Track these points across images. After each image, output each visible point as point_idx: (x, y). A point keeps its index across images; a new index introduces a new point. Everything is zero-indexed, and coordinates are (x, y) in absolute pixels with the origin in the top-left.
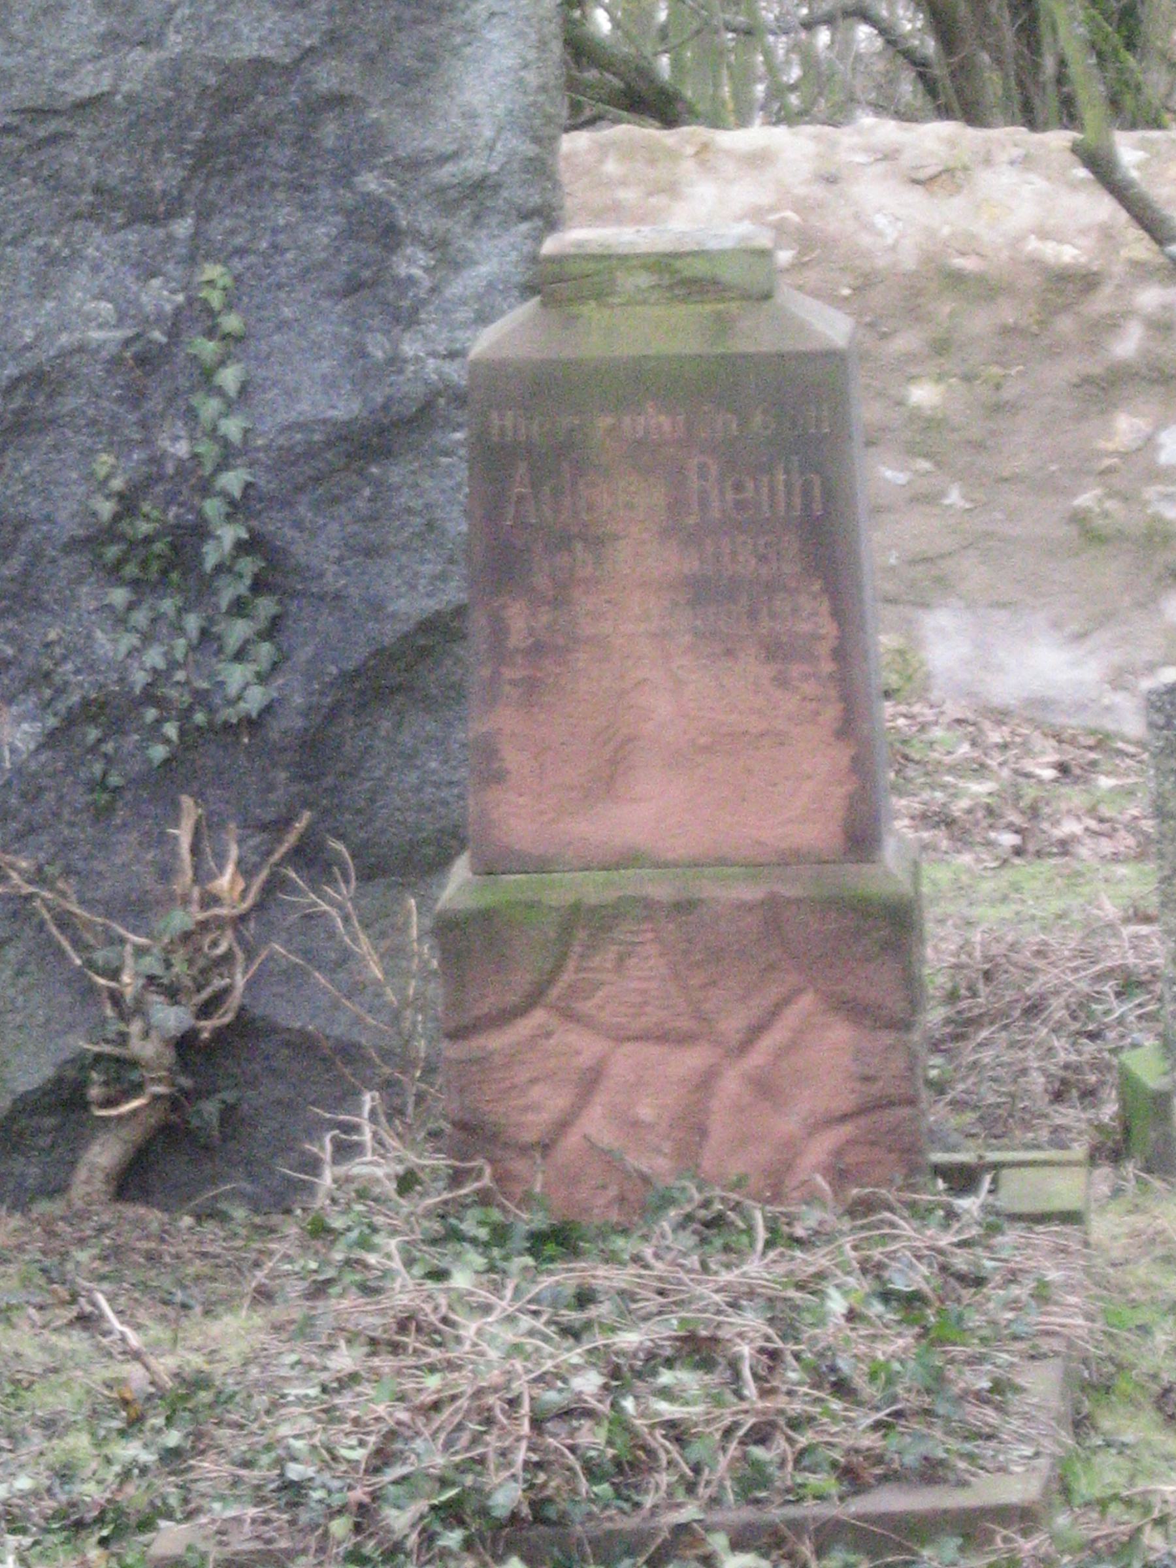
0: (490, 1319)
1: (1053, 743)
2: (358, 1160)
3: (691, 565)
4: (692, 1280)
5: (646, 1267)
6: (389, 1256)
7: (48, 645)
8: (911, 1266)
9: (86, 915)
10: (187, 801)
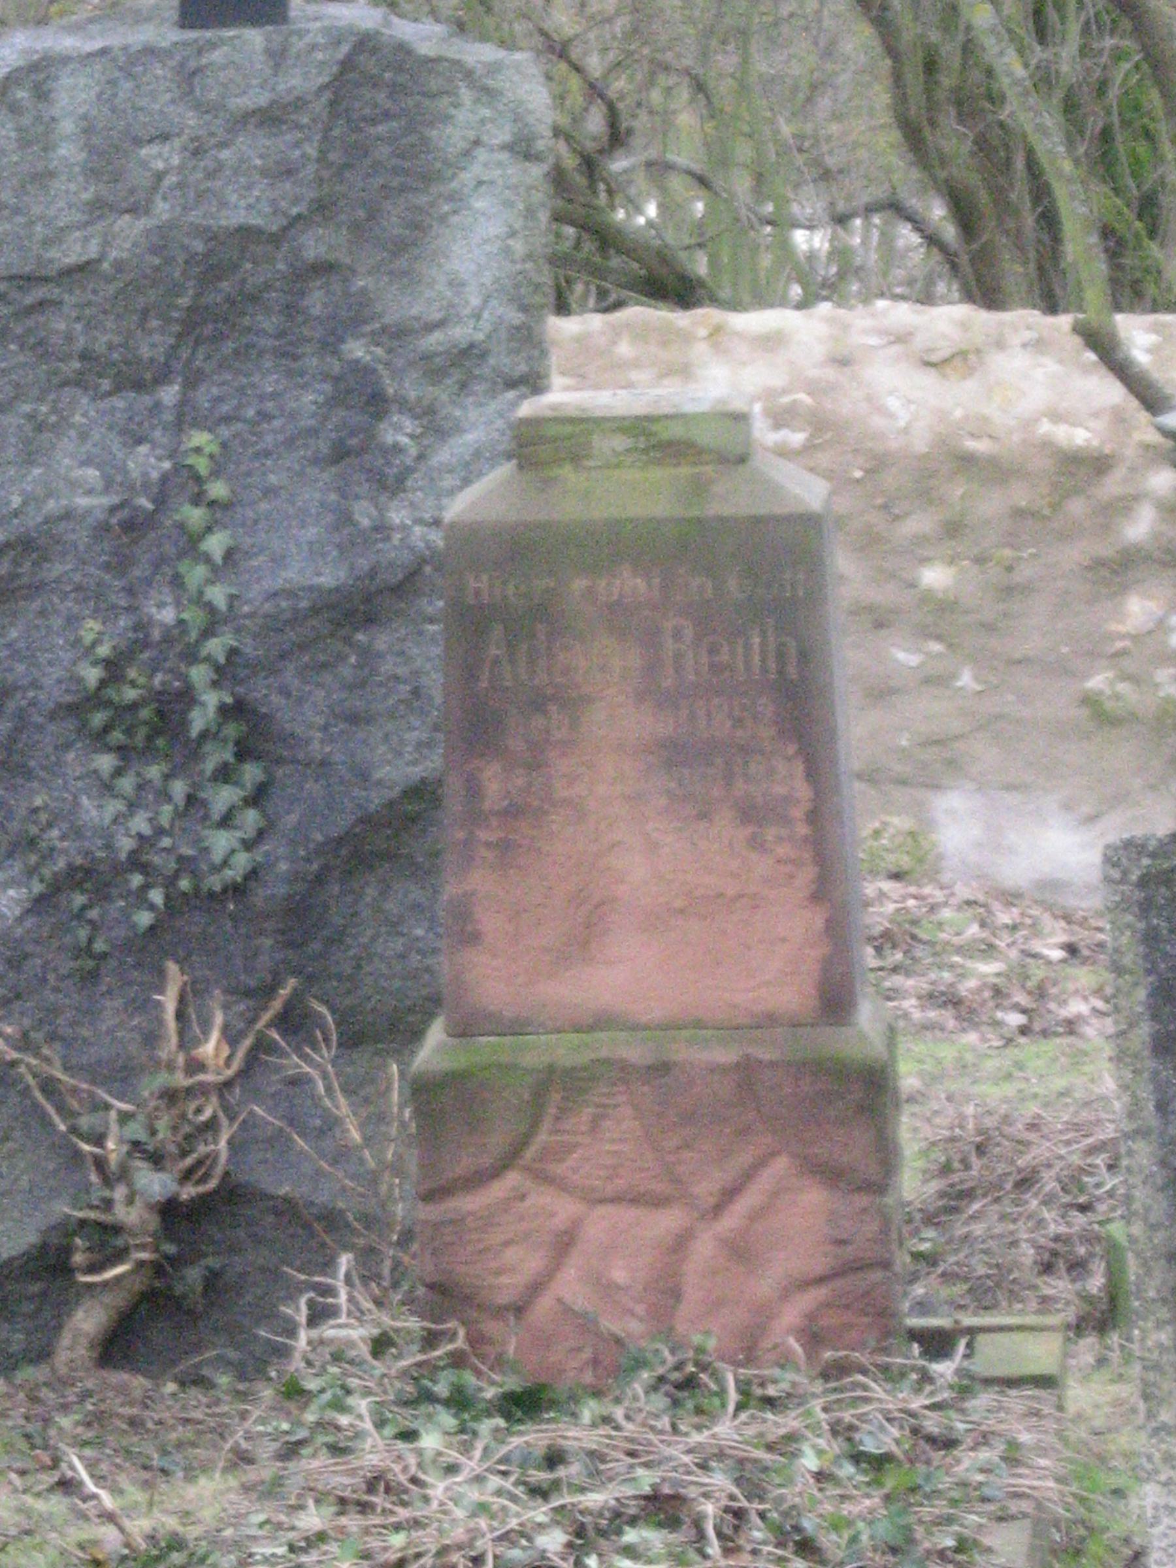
0: (458, 1479)
1: (1063, 924)
2: (332, 1322)
3: (662, 727)
4: (662, 1441)
5: (617, 1428)
6: (360, 1417)
7: (35, 811)
8: (882, 1428)
9: (72, 1081)
10: (172, 967)
